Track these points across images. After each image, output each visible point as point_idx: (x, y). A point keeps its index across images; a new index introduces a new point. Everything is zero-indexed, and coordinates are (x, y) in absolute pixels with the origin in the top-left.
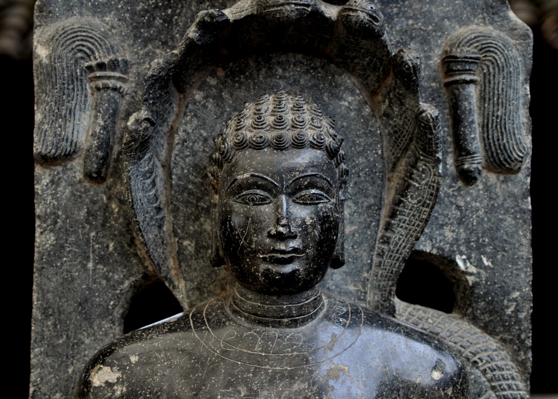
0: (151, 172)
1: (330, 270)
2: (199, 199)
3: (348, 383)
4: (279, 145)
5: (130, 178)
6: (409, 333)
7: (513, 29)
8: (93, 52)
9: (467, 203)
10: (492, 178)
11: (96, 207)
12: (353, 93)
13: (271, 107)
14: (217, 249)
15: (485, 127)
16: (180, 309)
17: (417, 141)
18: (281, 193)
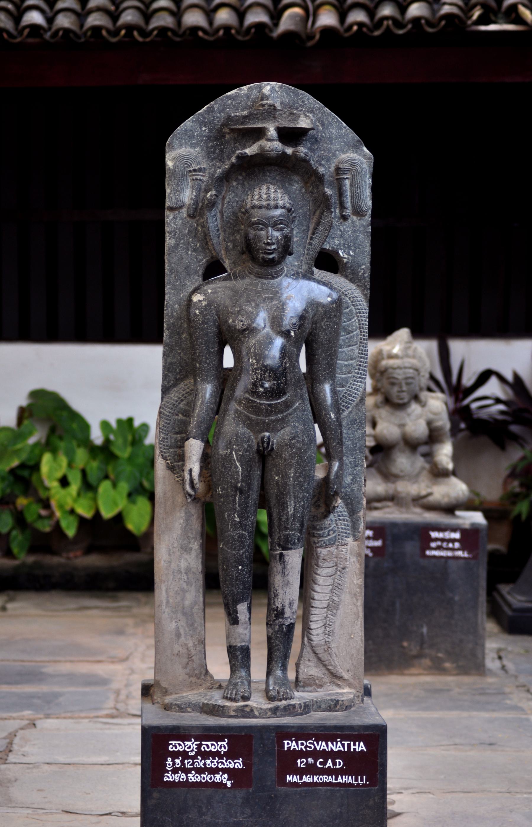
0: (215, 215)
1: (288, 256)
2: (234, 226)
3: (294, 302)
4: (268, 207)
5: (207, 218)
6: (319, 282)
7: (365, 155)
8: (191, 165)
9: (344, 228)
10: (355, 218)
11: (192, 229)
12: (298, 183)
13: (265, 191)
14: (243, 248)
15: (352, 197)
16: (226, 272)
17: (323, 204)
18: (269, 226)
